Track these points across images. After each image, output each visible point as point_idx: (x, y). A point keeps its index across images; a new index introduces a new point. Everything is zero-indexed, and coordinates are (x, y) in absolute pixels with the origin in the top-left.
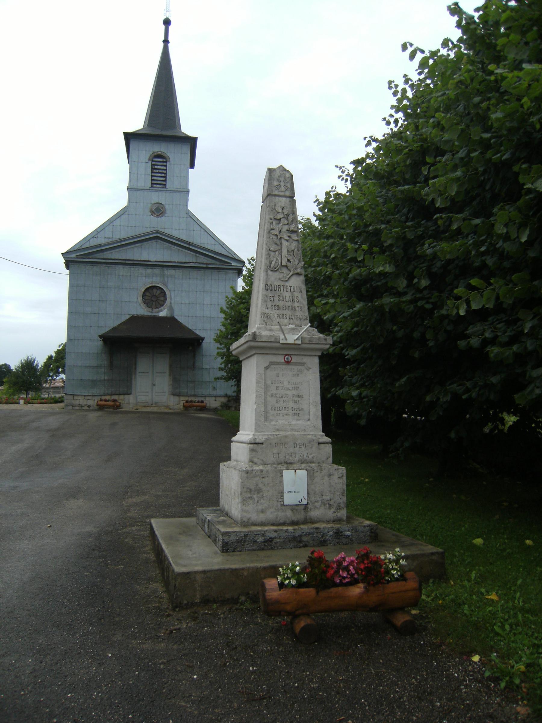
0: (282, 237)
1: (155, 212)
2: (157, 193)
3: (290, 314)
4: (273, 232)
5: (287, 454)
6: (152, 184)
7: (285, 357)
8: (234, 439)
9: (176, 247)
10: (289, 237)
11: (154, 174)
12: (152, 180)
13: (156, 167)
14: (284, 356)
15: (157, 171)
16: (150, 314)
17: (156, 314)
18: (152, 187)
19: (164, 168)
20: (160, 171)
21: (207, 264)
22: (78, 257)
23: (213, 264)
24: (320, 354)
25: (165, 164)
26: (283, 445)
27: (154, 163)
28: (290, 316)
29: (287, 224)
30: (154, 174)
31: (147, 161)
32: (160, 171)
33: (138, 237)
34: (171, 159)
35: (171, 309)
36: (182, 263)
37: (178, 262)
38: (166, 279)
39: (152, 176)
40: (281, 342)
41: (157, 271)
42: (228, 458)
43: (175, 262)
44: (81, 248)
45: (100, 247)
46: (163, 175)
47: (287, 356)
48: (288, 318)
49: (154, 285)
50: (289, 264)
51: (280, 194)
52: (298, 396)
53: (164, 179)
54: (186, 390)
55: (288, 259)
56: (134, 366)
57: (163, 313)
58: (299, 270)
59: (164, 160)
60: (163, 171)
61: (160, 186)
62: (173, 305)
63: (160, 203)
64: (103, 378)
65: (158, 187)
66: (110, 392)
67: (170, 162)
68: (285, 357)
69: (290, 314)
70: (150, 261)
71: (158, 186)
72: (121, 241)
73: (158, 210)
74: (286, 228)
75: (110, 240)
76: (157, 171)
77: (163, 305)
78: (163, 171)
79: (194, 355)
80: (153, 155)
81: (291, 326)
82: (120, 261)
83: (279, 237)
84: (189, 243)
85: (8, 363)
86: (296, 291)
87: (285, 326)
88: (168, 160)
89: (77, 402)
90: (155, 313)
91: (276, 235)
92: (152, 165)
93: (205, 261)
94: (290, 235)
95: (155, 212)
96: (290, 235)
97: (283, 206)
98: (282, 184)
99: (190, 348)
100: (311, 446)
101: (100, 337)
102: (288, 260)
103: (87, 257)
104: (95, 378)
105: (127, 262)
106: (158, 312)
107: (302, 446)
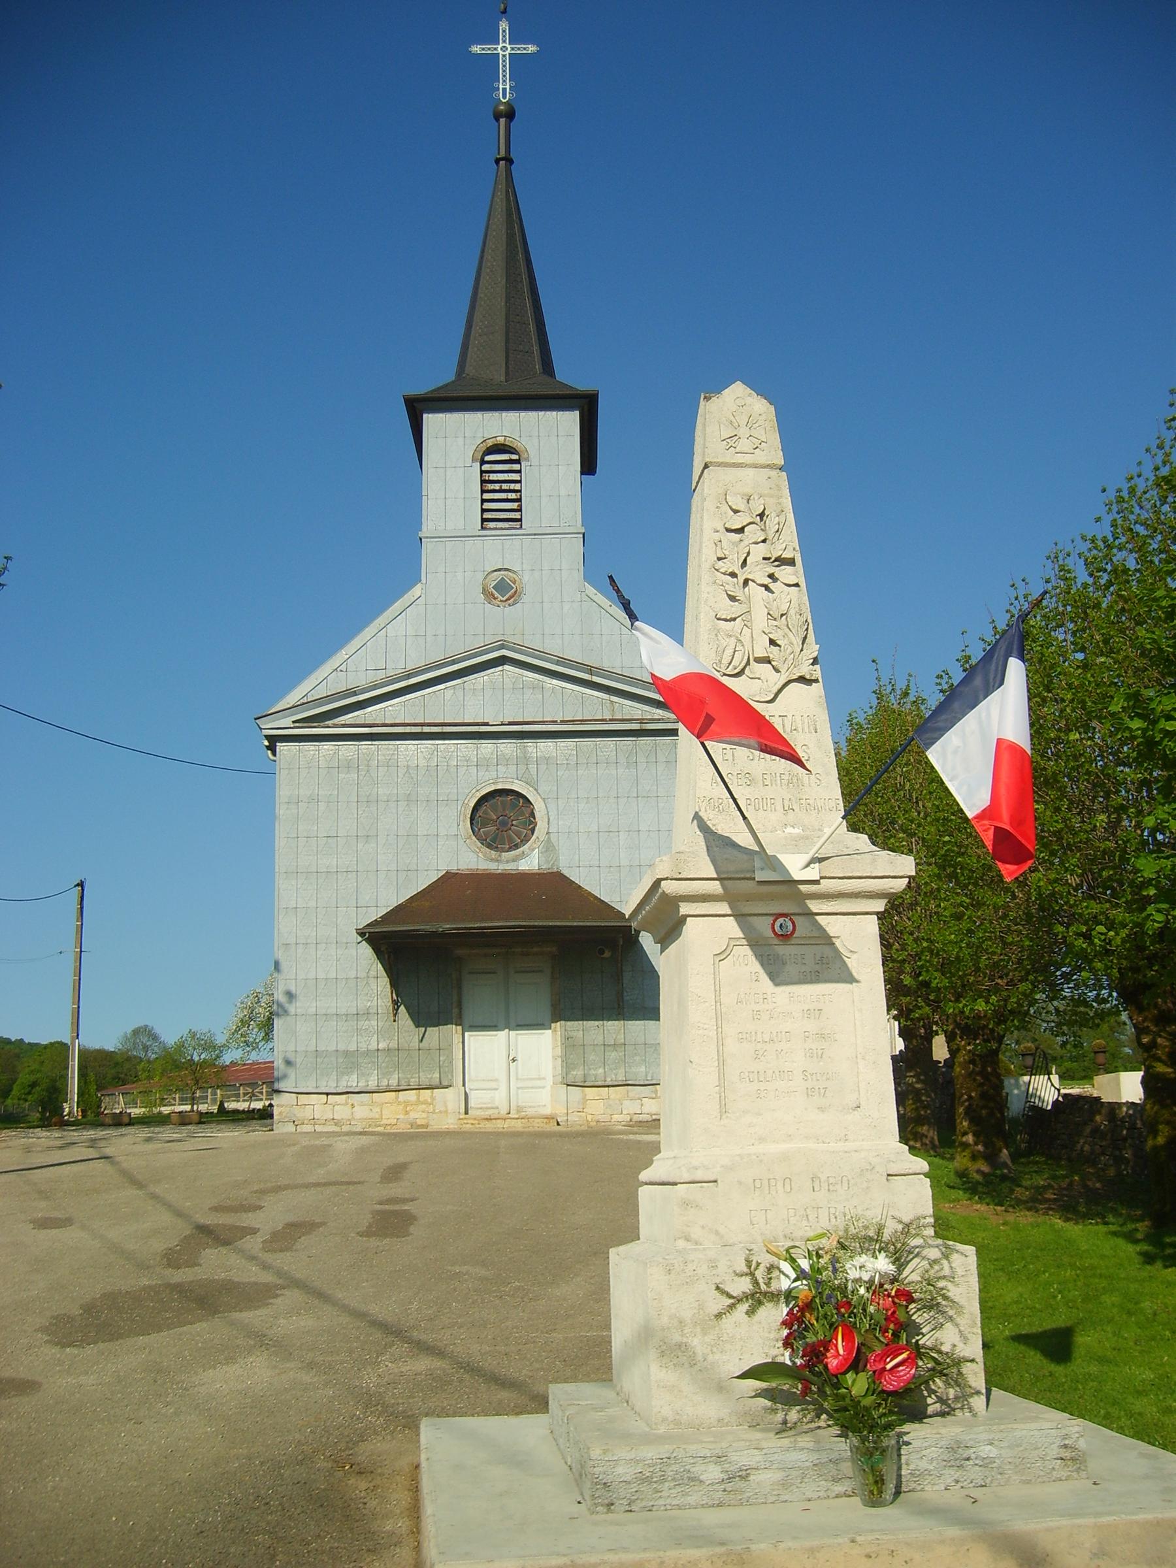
0: (750, 577)
1: (497, 595)
2: (498, 543)
3: (787, 797)
4: (724, 566)
5: (792, 1212)
6: (483, 520)
7: (774, 921)
8: (644, 1176)
9: (555, 682)
10: (771, 576)
11: (487, 496)
12: (483, 511)
13: (493, 477)
14: (770, 919)
15: (497, 487)
16: (492, 867)
17: (509, 867)
18: (483, 528)
19: (515, 477)
20: (505, 486)
21: (641, 721)
22: (297, 725)
23: (658, 721)
24: (880, 905)
25: (516, 467)
26: (780, 1184)
27: (486, 467)
28: (786, 803)
29: (764, 541)
30: (487, 496)
31: (469, 462)
32: (505, 486)
33: (454, 662)
34: (532, 453)
35: (549, 848)
36: (573, 722)
37: (563, 722)
38: (533, 768)
39: (483, 501)
40: (760, 876)
41: (507, 747)
42: (630, 1233)
43: (554, 722)
44: (305, 700)
45: (355, 694)
46: (490, 487)
47: (781, 920)
48: (779, 807)
49: (500, 787)
50: (774, 652)
51: (739, 459)
52: (822, 1036)
53: (515, 505)
54: (601, 1071)
55: (770, 639)
56: (455, 1011)
57: (530, 860)
58: (805, 670)
59: (515, 457)
60: (513, 486)
61: (506, 525)
62: (553, 838)
63: (506, 570)
64: (374, 1046)
65: (502, 529)
66: (394, 1082)
67: (527, 459)
68: (774, 921)
69: (787, 797)
70: (487, 724)
71: (500, 525)
72: (409, 677)
73: (502, 586)
74: (759, 551)
75: (381, 675)
76: (497, 487)
77: (525, 840)
78: (513, 486)
79: (618, 977)
80: (483, 448)
81: (789, 830)
82: (408, 730)
83: (741, 579)
84: (590, 670)
85: (150, 1024)
86: (800, 729)
87: (774, 830)
88: (524, 456)
89: (307, 1113)
90: (507, 862)
91: (733, 575)
92: (482, 472)
93: (638, 715)
94: (771, 570)
95: (497, 595)
96: (771, 570)
97: (748, 490)
98: (743, 432)
99: (607, 954)
100: (865, 1184)
101: (361, 933)
102: (772, 642)
103: (322, 724)
104: (353, 1047)
105: (426, 729)
106: (515, 859)
107: (838, 1187)
